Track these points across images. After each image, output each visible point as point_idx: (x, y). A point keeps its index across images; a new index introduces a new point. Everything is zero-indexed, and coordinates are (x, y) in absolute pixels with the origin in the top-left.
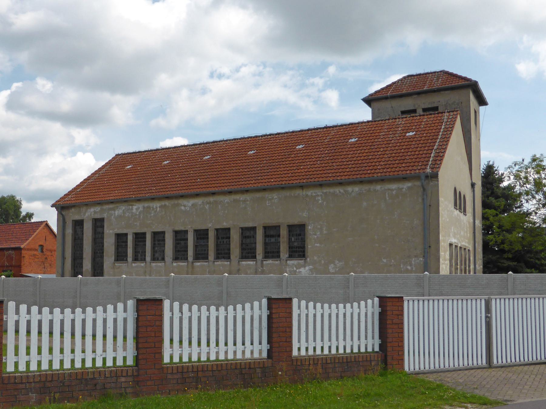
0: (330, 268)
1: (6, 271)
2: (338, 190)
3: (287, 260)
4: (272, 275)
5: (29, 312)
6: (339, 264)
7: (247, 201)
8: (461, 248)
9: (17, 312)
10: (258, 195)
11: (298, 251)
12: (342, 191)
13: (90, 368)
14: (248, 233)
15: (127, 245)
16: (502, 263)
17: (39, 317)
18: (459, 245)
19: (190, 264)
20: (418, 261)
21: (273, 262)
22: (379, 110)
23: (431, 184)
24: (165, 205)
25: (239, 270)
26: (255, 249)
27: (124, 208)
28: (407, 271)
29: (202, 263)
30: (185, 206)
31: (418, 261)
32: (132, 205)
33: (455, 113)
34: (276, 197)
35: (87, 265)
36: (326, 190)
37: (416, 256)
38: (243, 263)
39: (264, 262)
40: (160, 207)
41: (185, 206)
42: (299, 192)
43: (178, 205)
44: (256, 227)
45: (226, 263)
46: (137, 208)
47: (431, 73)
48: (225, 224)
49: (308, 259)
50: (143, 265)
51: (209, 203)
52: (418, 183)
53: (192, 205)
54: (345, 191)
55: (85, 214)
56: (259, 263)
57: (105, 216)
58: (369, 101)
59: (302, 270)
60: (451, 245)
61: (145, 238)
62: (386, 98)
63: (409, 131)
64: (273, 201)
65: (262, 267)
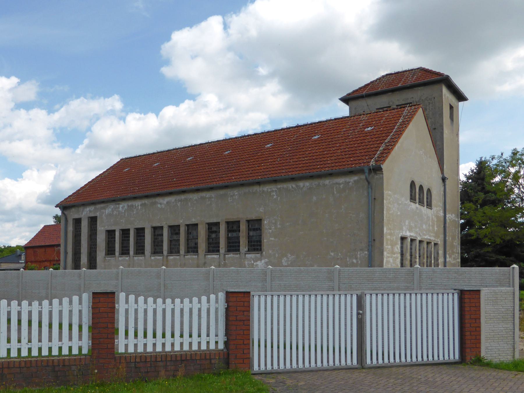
0: (283, 261)
1: (54, 265)
2: (291, 185)
3: (245, 254)
4: (233, 268)
5: (146, 302)
6: (291, 257)
7: (212, 198)
8: (421, 242)
9: (127, 302)
10: (222, 192)
11: (255, 246)
12: (294, 186)
13: (15, 358)
14: (213, 228)
15: (115, 241)
16: (490, 257)
17: (199, 306)
18: (419, 238)
19: (165, 258)
20: (363, 254)
21: (234, 255)
22: (356, 109)
23: (376, 177)
24: (145, 203)
25: (205, 263)
26: (219, 243)
27: (112, 207)
28: (353, 265)
29: (175, 257)
30: (161, 204)
31: (363, 254)
32: (119, 204)
33: (417, 107)
34: (236, 193)
35: (84, 259)
36: (280, 186)
37: (361, 250)
38: (209, 256)
39: (226, 256)
40: (141, 205)
41: (161, 204)
42: (256, 188)
43: (156, 203)
44: (219, 223)
45: (194, 257)
46: (123, 206)
47: (409, 71)
48: (193, 220)
49: (264, 253)
50: (127, 258)
51: (181, 201)
52: (363, 177)
53: (167, 203)
54: (297, 186)
55: (82, 214)
56: (222, 256)
57: (98, 214)
58: (346, 100)
59: (259, 263)
60: (403, 239)
61: (129, 234)
62: (362, 97)
63: (369, 126)
64: (234, 197)
65: (225, 260)
